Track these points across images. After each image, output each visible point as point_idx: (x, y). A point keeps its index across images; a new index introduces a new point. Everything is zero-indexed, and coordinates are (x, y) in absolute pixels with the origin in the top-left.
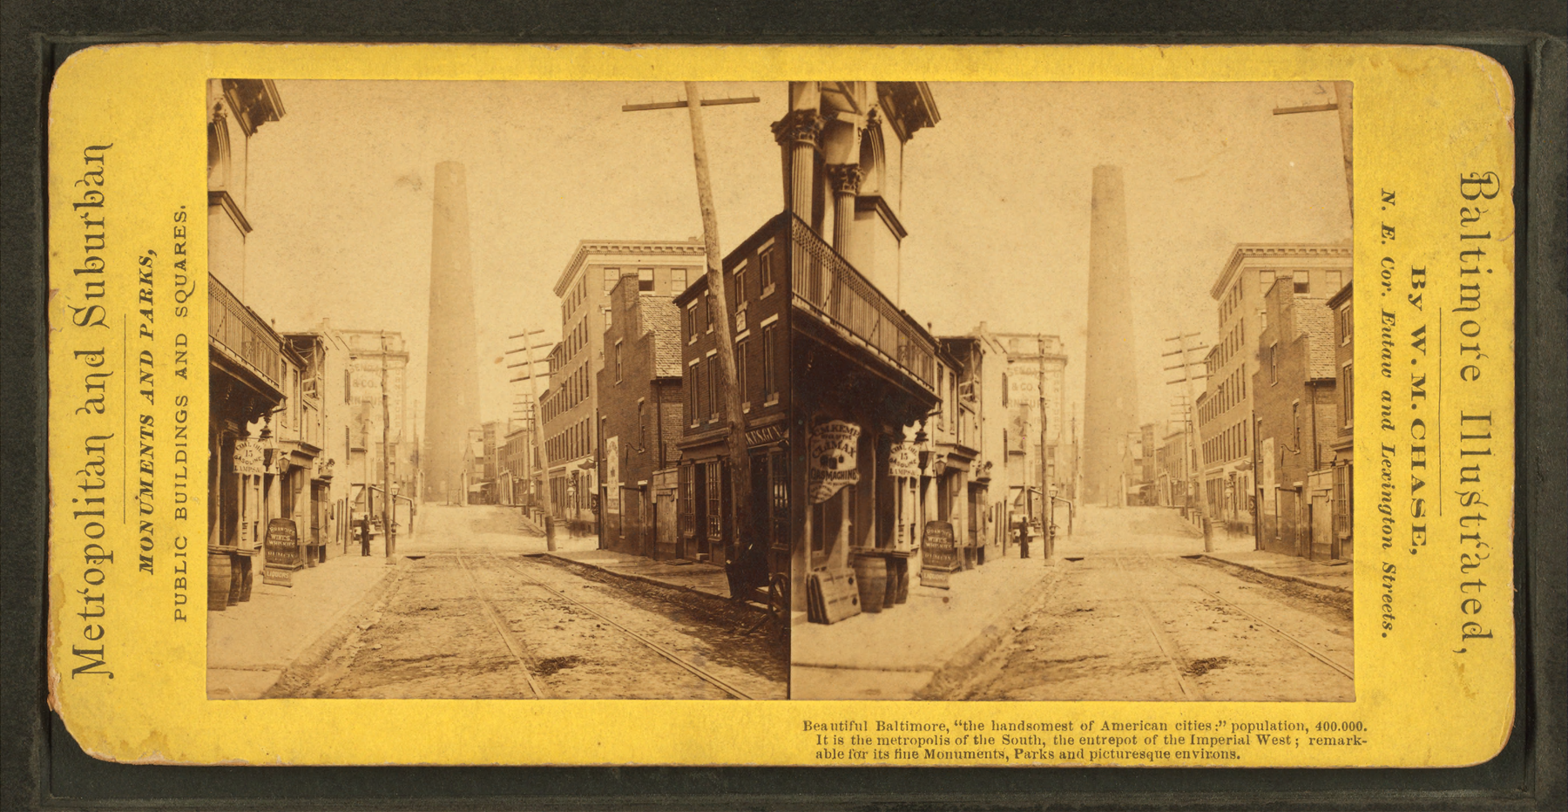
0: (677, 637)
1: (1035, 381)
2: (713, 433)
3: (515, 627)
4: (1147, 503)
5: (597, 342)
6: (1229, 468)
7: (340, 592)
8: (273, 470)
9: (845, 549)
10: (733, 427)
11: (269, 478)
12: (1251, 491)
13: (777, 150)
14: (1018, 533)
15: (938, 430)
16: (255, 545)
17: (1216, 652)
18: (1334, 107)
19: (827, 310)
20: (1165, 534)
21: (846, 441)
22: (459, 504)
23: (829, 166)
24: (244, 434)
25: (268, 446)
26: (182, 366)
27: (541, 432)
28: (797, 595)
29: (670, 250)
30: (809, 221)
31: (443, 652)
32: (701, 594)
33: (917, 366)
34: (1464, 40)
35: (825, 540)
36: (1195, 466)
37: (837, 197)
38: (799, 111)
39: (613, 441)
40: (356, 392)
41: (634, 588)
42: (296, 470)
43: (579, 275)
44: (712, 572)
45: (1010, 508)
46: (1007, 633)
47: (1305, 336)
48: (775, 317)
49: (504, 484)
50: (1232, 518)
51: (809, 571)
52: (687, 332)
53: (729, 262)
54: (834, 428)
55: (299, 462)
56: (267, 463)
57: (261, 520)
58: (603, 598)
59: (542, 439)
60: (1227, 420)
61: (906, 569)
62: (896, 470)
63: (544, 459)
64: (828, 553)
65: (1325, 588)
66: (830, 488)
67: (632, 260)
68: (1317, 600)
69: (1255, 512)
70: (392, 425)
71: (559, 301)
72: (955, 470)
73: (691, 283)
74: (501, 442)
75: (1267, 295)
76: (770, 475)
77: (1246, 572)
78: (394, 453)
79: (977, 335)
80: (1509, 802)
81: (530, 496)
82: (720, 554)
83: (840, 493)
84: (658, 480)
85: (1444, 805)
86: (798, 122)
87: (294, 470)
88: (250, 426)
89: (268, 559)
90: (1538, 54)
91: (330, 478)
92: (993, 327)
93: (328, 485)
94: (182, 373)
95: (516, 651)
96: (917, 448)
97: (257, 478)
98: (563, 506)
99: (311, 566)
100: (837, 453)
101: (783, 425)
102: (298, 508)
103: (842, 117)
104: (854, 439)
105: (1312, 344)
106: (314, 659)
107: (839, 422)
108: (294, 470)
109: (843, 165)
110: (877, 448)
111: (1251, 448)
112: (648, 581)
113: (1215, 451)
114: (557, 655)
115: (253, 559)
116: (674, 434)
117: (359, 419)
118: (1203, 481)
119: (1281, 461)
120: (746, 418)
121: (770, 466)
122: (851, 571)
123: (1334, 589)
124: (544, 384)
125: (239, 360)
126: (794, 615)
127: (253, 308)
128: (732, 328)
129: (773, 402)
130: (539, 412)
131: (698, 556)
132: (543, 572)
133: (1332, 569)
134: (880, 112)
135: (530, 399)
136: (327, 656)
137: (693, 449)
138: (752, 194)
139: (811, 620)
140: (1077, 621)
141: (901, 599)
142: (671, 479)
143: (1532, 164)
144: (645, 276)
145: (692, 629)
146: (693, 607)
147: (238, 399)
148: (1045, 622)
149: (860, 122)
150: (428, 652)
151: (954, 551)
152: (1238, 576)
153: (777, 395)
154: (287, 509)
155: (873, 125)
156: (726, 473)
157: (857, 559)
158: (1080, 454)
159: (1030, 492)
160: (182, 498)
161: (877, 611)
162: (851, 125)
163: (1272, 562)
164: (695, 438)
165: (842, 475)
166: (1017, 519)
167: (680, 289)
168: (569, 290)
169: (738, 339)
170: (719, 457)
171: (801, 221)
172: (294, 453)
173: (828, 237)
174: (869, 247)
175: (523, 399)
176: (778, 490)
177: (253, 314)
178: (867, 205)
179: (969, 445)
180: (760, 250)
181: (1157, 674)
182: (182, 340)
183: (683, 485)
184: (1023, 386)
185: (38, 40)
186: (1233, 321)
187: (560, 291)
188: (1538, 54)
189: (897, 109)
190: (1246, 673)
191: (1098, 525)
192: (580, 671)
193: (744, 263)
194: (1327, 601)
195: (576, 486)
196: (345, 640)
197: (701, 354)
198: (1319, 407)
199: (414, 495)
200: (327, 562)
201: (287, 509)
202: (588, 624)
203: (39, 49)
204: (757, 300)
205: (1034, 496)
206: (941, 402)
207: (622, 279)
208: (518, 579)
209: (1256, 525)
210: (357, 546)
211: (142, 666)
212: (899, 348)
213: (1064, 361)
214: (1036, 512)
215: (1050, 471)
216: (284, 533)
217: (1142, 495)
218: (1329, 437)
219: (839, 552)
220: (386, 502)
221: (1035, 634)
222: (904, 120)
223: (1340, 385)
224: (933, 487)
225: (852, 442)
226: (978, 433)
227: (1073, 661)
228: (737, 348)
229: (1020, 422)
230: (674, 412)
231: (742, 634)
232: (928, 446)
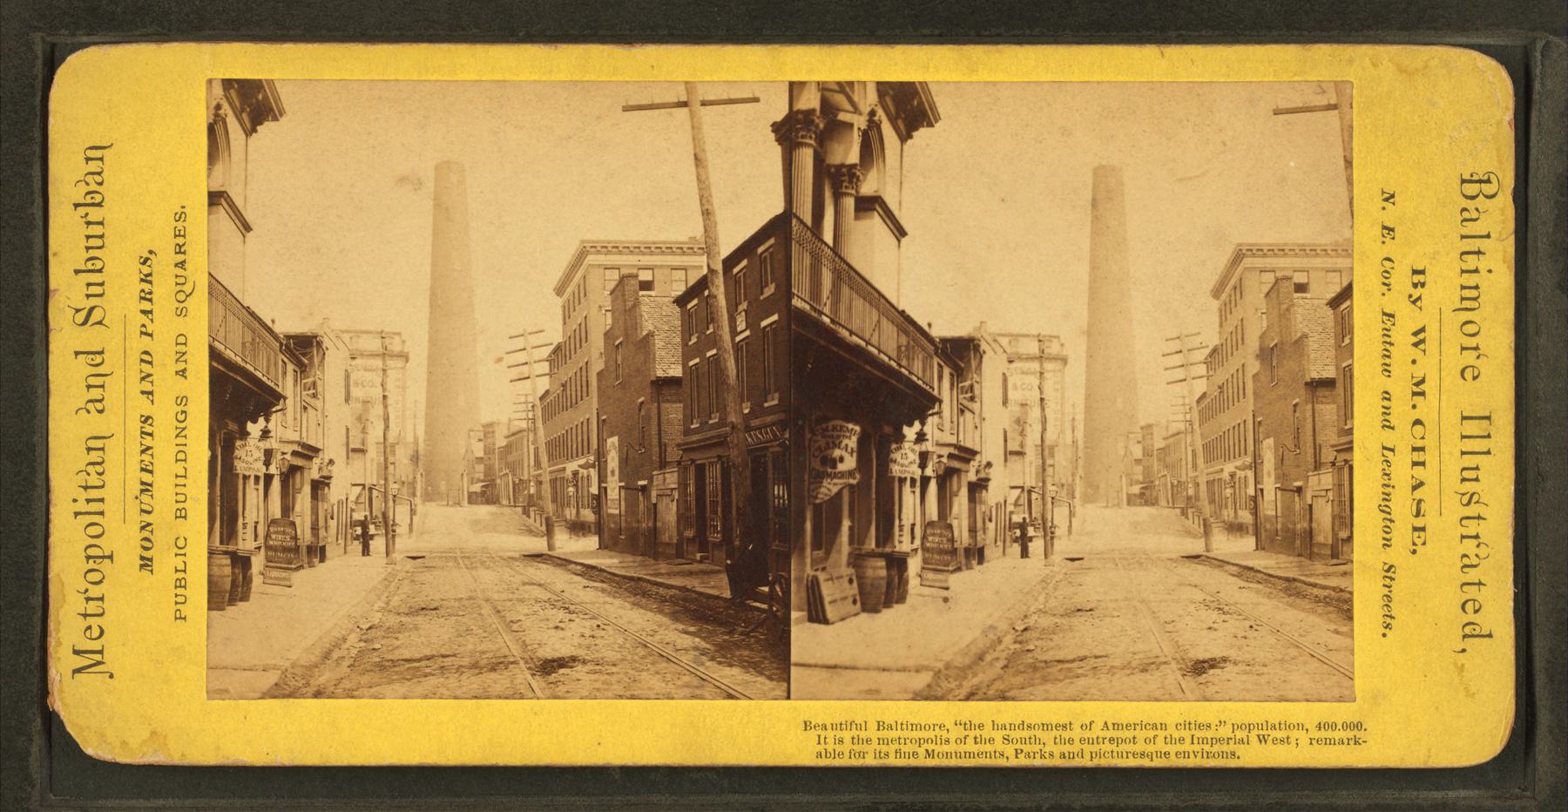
0: (677, 637)
1: (1035, 381)
2: (713, 433)
5: (597, 342)
6: (1229, 468)
7: (340, 592)
8: (273, 470)
9: (845, 549)
11: (269, 478)
12: (1251, 491)
13: (777, 151)
14: (1018, 532)
15: (938, 430)
19: (827, 310)
20: (1162, 533)
21: (846, 441)
22: (459, 504)
23: (829, 166)
24: (244, 434)
25: (268, 446)
26: (181, 366)
27: (541, 432)
28: (797, 595)
29: (670, 250)
30: (809, 221)
31: (443, 652)
32: (701, 594)
33: (917, 366)
34: (1464, 40)
35: (825, 540)
36: (1195, 466)
37: (837, 197)
38: (799, 112)
39: (613, 442)
40: (356, 392)
41: (634, 588)
42: (296, 470)
43: (579, 275)
44: (712, 572)
45: (1010, 508)
46: (1007, 633)
47: (1305, 336)
48: (775, 317)
50: (1232, 518)
51: (809, 571)
52: (687, 332)
53: (730, 262)
54: (834, 428)
55: (299, 462)
56: (267, 464)
57: (261, 520)
59: (542, 440)
60: (1227, 420)
62: (896, 470)
63: (544, 459)
64: (828, 553)
65: (1325, 588)
66: (830, 488)
67: (632, 260)
68: (1317, 600)
69: (1255, 512)
71: (559, 301)
72: (955, 470)
73: (691, 283)
74: (501, 442)
75: (1267, 295)
76: (770, 475)
77: (1246, 572)
78: (393, 453)
80: (1509, 803)
81: (530, 496)
82: (720, 554)
83: (840, 492)
84: (658, 480)
85: (1444, 805)
86: (798, 122)
87: (294, 470)
88: (250, 426)
89: (268, 559)
90: (1538, 55)
92: (993, 327)
93: (328, 485)
94: (182, 373)
95: (516, 651)
96: (917, 448)
97: (257, 478)
99: (311, 565)
100: (837, 453)
102: (298, 508)
103: (842, 117)
104: (854, 439)
106: (313, 659)
107: (839, 422)
108: (294, 470)
109: (843, 165)
110: (877, 448)
111: (594, 445)
113: (1215, 451)
114: (557, 655)
115: (253, 559)
116: (674, 434)
117: (359, 419)
118: (1203, 480)
119: (1281, 461)
122: (851, 571)
123: (1334, 589)
124: (544, 384)
126: (794, 615)
127: (253, 308)
128: (732, 328)
129: (773, 402)
130: (539, 412)
131: (698, 556)
132: (543, 572)
133: (1332, 569)
134: (880, 113)
136: (327, 656)
137: (693, 449)
138: (752, 194)
139: (811, 620)
140: (1077, 621)
141: (901, 599)
142: (671, 479)
143: (1532, 164)
144: (645, 276)
145: (692, 629)
146: (693, 607)
147: (238, 399)
148: (1046, 622)
149: (860, 122)
150: (428, 652)
151: (954, 552)
152: (1238, 576)
154: (287, 509)
155: (873, 124)
156: (726, 474)
157: (857, 560)
160: (182, 498)
161: (877, 611)
162: (851, 125)
164: (694, 438)
165: (842, 475)
166: (1017, 519)
167: (680, 289)
168: (569, 290)
169: (738, 339)
170: (719, 457)
171: (801, 222)
172: (294, 453)
173: (828, 237)
174: (869, 247)
175: (523, 399)
176: (778, 490)
177: (252, 314)
178: (867, 205)
179: (969, 445)
180: (760, 250)
181: (1158, 674)
182: (182, 340)
183: (683, 485)
184: (1023, 386)
185: (38, 40)
186: (1233, 321)
187: (559, 291)
188: (1538, 55)
191: (1098, 525)
192: (579, 671)
193: (745, 263)
194: (1327, 601)
195: (576, 486)
196: (345, 640)
197: (701, 354)
198: (1319, 407)
199: (414, 495)
200: (327, 562)
201: (287, 509)
202: (588, 624)
203: (39, 49)
204: (757, 300)
205: (1034, 496)
206: (941, 402)
207: (622, 279)
208: (518, 579)
209: (1256, 525)
210: (357, 546)
211: (142, 666)
212: (899, 347)
213: (1064, 360)
214: (1036, 512)
215: (1050, 471)
216: (284, 533)
218: (1329, 437)
219: (839, 552)
220: (386, 502)
221: (1035, 634)
223: (1340, 385)
224: (933, 487)
225: (852, 442)
226: (978, 433)
227: (1073, 661)
228: (737, 348)
229: (1020, 422)
230: (674, 412)
232: (928, 446)
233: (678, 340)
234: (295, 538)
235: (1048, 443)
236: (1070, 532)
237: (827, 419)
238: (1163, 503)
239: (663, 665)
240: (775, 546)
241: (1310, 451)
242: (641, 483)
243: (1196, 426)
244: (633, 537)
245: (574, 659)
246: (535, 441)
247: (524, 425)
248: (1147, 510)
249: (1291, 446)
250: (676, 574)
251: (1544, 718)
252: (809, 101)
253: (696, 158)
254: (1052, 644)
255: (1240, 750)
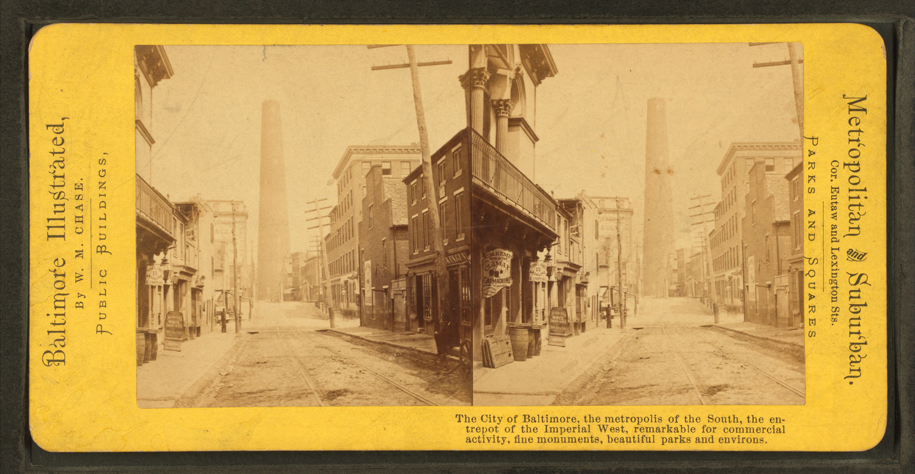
0: (405, 376)
1: (614, 224)
2: (427, 257)
3: (312, 372)
4: (680, 295)
5: (358, 206)
6: (728, 273)
7: (210, 352)
8: (169, 282)
10: (438, 253)
11: (166, 287)
12: (741, 287)
13: (462, 92)
14: (605, 313)
15: (558, 254)
16: (159, 327)
17: (721, 382)
18: (408, 66)
19: (492, 185)
20: (687, 313)
21: (504, 261)
22: (278, 301)
23: (492, 101)
24: (536, 258)
27: (710, 255)
28: (477, 352)
29: (401, 150)
31: (271, 388)
32: (420, 352)
33: (546, 215)
35: (492, 318)
36: (708, 273)
37: (498, 118)
38: (475, 69)
39: (368, 263)
40: (217, 237)
41: (384, 349)
42: (183, 282)
43: (731, 163)
44: (427, 339)
45: (600, 299)
47: (772, 197)
48: (462, 189)
49: (689, 283)
51: (483, 337)
52: (410, 200)
53: (435, 158)
54: (497, 254)
55: (184, 278)
56: (549, 275)
57: (547, 309)
58: (361, 354)
59: (326, 264)
60: (343, 250)
61: (156, 340)
62: (533, 278)
63: (328, 276)
64: (494, 326)
65: (785, 343)
66: (495, 288)
67: (378, 157)
68: (780, 351)
69: (744, 299)
70: (238, 255)
71: (719, 178)
72: (568, 278)
73: (413, 170)
74: (302, 264)
76: (460, 281)
77: (739, 335)
78: (239, 271)
79: (194, 201)
80: (885, 466)
81: (320, 296)
82: (431, 328)
83: (500, 292)
84: (395, 285)
85: (847, 468)
86: (475, 75)
87: (181, 282)
88: (539, 254)
89: (166, 335)
90: (901, 29)
91: (202, 287)
92: (589, 193)
93: (201, 291)
95: (312, 387)
96: (546, 264)
97: (160, 287)
98: (723, 296)
99: (192, 338)
100: (499, 268)
101: (467, 252)
103: (500, 71)
104: (509, 260)
105: (776, 200)
106: (194, 393)
107: (500, 250)
108: (181, 282)
109: (501, 100)
110: (522, 266)
111: (357, 266)
112: (772, 340)
113: (719, 264)
115: (158, 335)
116: (404, 259)
117: (604, 248)
118: (713, 281)
119: (758, 270)
120: (446, 248)
121: (460, 277)
122: (508, 337)
123: (790, 344)
125: (532, 216)
126: (475, 363)
127: (156, 188)
128: (436, 197)
129: (461, 238)
130: (324, 247)
131: (419, 329)
133: (407, 337)
134: (523, 70)
135: (703, 235)
136: (584, 387)
137: (414, 267)
138: (448, 119)
139: (484, 366)
140: (638, 364)
141: (537, 353)
142: (403, 285)
143: (898, 93)
144: (386, 166)
145: (415, 372)
146: (416, 359)
147: (151, 242)
148: (623, 366)
149: (511, 74)
150: (261, 388)
151: (184, 329)
152: (350, 342)
153: (463, 235)
155: (518, 75)
156: (434, 281)
157: (511, 331)
158: (641, 267)
159: (612, 289)
162: (505, 76)
163: (753, 329)
164: (416, 260)
165: (502, 281)
166: (604, 305)
167: (406, 174)
169: (441, 202)
170: (430, 271)
171: (477, 133)
172: (181, 273)
173: (493, 142)
174: (517, 148)
175: (315, 239)
177: (156, 192)
178: (515, 123)
179: (192, 267)
180: (453, 150)
181: (687, 395)
183: (409, 288)
184: (223, 232)
186: (346, 192)
187: (720, 172)
188: (901, 29)
189: (532, 66)
190: (739, 393)
191: (652, 309)
192: (729, 393)
193: (444, 158)
194: (786, 351)
195: (347, 289)
196: (212, 382)
197: (418, 211)
199: (637, 292)
202: (354, 370)
203: (23, 27)
205: (614, 292)
206: (559, 237)
207: (373, 169)
208: (314, 344)
209: (744, 307)
210: (219, 327)
214: (230, 306)
215: (623, 277)
216: (176, 319)
217: (292, 294)
218: (786, 255)
219: (501, 326)
220: (235, 300)
221: (615, 372)
222: (537, 73)
223: (792, 225)
224: (555, 287)
225: (508, 262)
226: (581, 255)
227: (638, 388)
228: (440, 207)
229: (606, 248)
230: (403, 245)
231: (445, 374)
232: (552, 263)
233: (406, 203)
234: (183, 323)
235: (622, 261)
236: (250, 317)
237: (494, 249)
238: (305, 299)
239: (398, 394)
240: (464, 323)
241: (776, 263)
242: (385, 287)
243: (325, 254)
244: (386, 319)
245: (346, 391)
246: (323, 263)
247: (315, 254)
248: (297, 303)
249: (765, 261)
250: (406, 340)
251: (905, 417)
252: (481, 62)
253: (415, 97)
254: (242, 383)
255: (765, 436)
